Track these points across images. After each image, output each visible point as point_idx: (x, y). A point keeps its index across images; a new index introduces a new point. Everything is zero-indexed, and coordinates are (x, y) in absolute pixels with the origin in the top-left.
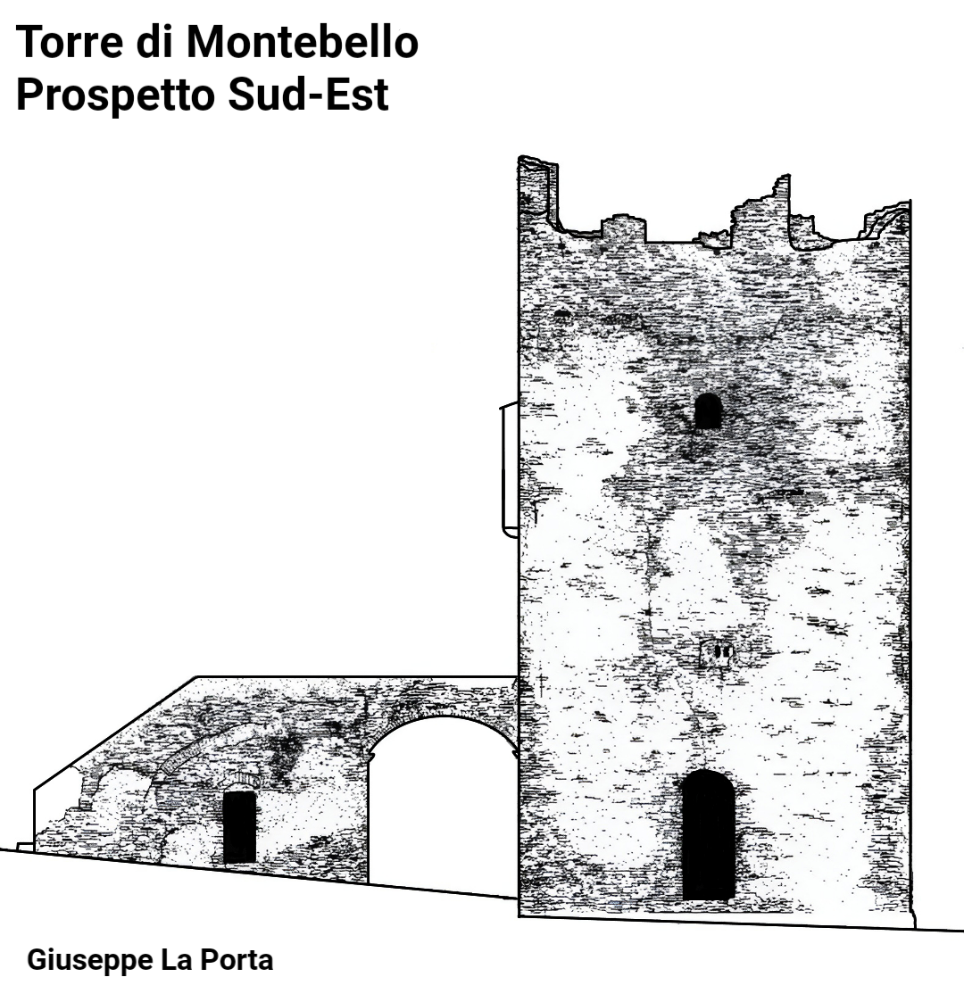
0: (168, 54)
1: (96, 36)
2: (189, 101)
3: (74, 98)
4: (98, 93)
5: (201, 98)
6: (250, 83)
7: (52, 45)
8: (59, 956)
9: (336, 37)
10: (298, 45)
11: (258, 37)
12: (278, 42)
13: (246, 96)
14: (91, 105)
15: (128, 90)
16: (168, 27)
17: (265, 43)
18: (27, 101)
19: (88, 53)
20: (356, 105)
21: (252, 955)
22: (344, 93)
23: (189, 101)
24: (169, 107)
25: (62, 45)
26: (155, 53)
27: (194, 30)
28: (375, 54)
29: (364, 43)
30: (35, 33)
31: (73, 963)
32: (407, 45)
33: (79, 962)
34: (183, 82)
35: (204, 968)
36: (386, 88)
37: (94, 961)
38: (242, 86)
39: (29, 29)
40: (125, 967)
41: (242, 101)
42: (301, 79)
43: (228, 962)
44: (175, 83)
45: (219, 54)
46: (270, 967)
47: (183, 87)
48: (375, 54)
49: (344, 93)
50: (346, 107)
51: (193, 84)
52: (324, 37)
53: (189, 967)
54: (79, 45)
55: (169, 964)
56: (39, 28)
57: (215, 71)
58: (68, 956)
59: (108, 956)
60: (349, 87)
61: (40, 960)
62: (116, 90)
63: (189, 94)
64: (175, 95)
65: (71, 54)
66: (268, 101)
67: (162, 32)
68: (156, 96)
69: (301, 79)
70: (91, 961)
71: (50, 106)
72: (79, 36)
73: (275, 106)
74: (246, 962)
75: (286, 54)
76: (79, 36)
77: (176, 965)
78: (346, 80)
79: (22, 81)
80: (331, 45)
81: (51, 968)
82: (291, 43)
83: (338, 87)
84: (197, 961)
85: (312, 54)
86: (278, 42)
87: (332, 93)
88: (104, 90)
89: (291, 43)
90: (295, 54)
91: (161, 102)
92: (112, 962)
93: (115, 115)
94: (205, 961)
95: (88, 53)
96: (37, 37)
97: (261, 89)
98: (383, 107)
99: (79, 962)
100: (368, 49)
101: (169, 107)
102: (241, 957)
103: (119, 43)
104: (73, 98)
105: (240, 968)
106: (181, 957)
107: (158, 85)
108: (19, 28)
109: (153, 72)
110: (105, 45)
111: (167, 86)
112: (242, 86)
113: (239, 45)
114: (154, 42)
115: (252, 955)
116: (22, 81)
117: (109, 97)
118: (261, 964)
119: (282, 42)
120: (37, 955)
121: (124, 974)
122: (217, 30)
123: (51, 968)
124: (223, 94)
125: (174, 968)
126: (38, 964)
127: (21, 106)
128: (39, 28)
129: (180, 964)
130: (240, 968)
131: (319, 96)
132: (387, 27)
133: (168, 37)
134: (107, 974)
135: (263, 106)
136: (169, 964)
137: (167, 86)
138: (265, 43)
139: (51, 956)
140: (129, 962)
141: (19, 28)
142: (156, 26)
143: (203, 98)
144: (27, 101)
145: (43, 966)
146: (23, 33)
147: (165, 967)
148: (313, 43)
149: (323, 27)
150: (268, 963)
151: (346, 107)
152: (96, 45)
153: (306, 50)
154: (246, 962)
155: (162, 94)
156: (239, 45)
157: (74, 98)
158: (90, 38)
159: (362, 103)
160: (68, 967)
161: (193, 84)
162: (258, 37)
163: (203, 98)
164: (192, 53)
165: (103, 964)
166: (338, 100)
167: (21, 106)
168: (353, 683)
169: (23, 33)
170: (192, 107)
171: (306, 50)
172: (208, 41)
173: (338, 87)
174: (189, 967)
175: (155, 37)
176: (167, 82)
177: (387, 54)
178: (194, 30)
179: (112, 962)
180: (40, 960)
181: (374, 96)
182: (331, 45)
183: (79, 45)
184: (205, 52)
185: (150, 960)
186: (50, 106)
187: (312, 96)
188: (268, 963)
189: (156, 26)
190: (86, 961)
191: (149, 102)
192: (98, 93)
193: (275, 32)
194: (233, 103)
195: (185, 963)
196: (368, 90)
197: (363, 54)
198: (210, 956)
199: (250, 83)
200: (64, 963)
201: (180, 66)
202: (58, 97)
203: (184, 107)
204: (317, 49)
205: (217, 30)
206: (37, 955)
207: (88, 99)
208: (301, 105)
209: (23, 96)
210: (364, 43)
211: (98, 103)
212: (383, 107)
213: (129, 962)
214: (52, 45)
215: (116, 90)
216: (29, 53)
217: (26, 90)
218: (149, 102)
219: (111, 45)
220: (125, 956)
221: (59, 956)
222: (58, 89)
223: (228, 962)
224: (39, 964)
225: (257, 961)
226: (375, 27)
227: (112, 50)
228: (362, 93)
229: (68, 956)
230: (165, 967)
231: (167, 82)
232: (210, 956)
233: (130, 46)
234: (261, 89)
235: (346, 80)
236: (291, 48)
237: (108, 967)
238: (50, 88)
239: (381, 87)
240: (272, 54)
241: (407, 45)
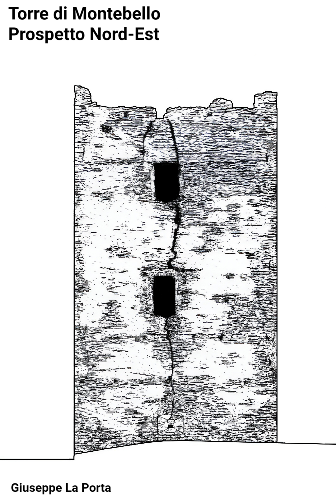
0: (65, 18)
2: (75, 37)
3: (30, 35)
4: (40, 33)
5: (78, 35)
7: (22, 15)
11: (99, 12)
12: (107, 13)
13: (96, 34)
14: (37, 38)
16: (65, 8)
17: (102, 14)
19: (36, 18)
20: (146, 38)
21: (103, 486)
22: (142, 33)
23: (75, 37)
25: (26, 15)
26: (61, 18)
27: (75, 9)
28: (144, 18)
30: (16, 10)
31: (29, 489)
32: (156, 15)
33: (32, 489)
35: (83, 491)
36: (158, 31)
37: (38, 488)
39: (14, 9)
40: (50, 491)
42: (125, 28)
44: (69, 30)
45: (85, 18)
46: (110, 491)
47: (72, 31)
48: (144, 18)
49: (142, 33)
50: (143, 39)
51: (76, 30)
52: (125, 11)
53: (77, 491)
54: (32, 15)
56: (17, 8)
57: (84, 25)
59: (44, 486)
60: (144, 31)
62: (47, 32)
63: (75, 34)
64: (69, 35)
67: (63, 10)
68: (62, 35)
69: (125, 28)
70: (37, 489)
71: (22, 38)
74: (100, 488)
75: (110, 18)
76: (32, 11)
77: (71, 490)
78: (143, 28)
79: (11, 29)
80: (127, 15)
81: (21, 491)
82: (112, 14)
83: (140, 31)
85: (120, 18)
86: (107, 13)
87: (137, 33)
88: (42, 32)
89: (112, 14)
90: (113, 18)
91: (64, 37)
94: (83, 488)
95: (36, 18)
96: (17, 11)
98: (157, 39)
99: (32, 489)
100: (141, 17)
103: (47, 14)
104: (30, 35)
105: (97, 491)
107: (63, 30)
108: (10, 8)
110: (41, 15)
111: (66, 31)
113: (92, 15)
114: (60, 14)
115: (103, 486)
116: (11, 29)
117: (44, 35)
119: (109, 14)
120: (15, 486)
121: (50, 493)
122: (84, 9)
123: (21, 491)
124: (88, 34)
126: (15, 489)
127: (11, 39)
128: (17, 8)
130: (97, 491)
131: (132, 35)
133: (65, 12)
134: (43, 493)
137: (66, 31)
138: (102, 14)
139: (21, 486)
141: (10, 8)
142: (61, 8)
143: (80, 35)
146: (11, 10)
147: (67, 491)
149: (124, 8)
150: (109, 489)
151: (143, 39)
154: (100, 488)
155: (64, 34)
156: (92, 15)
157: (30, 35)
158: (36, 12)
159: (149, 37)
160: (27, 491)
161: (76, 30)
162: (99, 12)
163: (80, 35)
164: (74, 18)
165: (42, 490)
166: (140, 36)
167: (11, 39)
169: (11, 10)
170: (76, 39)
171: (118, 17)
172: (81, 13)
173: (140, 31)
174: (77, 491)
175: (60, 12)
176: (66, 29)
177: (148, 18)
178: (75, 9)
181: (153, 35)
182: (127, 15)
183: (32, 15)
184: (80, 18)
186: (22, 38)
187: (130, 35)
188: (109, 489)
189: (61, 8)
190: (35, 488)
192: (40, 33)
193: (106, 10)
195: (75, 489)
196: (151, 32)
197: (139, 18)
200: (26, 489)
201: (70, 23)
202: (24, 35)
203: (73, 39)
204: (122, 17)
205: (84, 9)
206: (15, 486)
207: (36, 36)
208: (125, 38)
210: (140, 14)
211: (40, 37)
212: (157, 39)
214: (22, 15)
215: (47, 32)
216: (14, 18)
217: (12, 32)
219: (44, 15)
220: (50, 486)
221: (24, 486)
224: (16, 490)
225: (104, 488)
226: (144, 8)
227: (44, 17)
228: (149, 33)
229: (28, 486)
230: (67, 491)
232: (14, 31)
233: (51, 15)
235: (143, 28)
236: (112, 16)
237: (44, 491)
239: (156, 31)
240: (105, 18)
241: (156, 15)
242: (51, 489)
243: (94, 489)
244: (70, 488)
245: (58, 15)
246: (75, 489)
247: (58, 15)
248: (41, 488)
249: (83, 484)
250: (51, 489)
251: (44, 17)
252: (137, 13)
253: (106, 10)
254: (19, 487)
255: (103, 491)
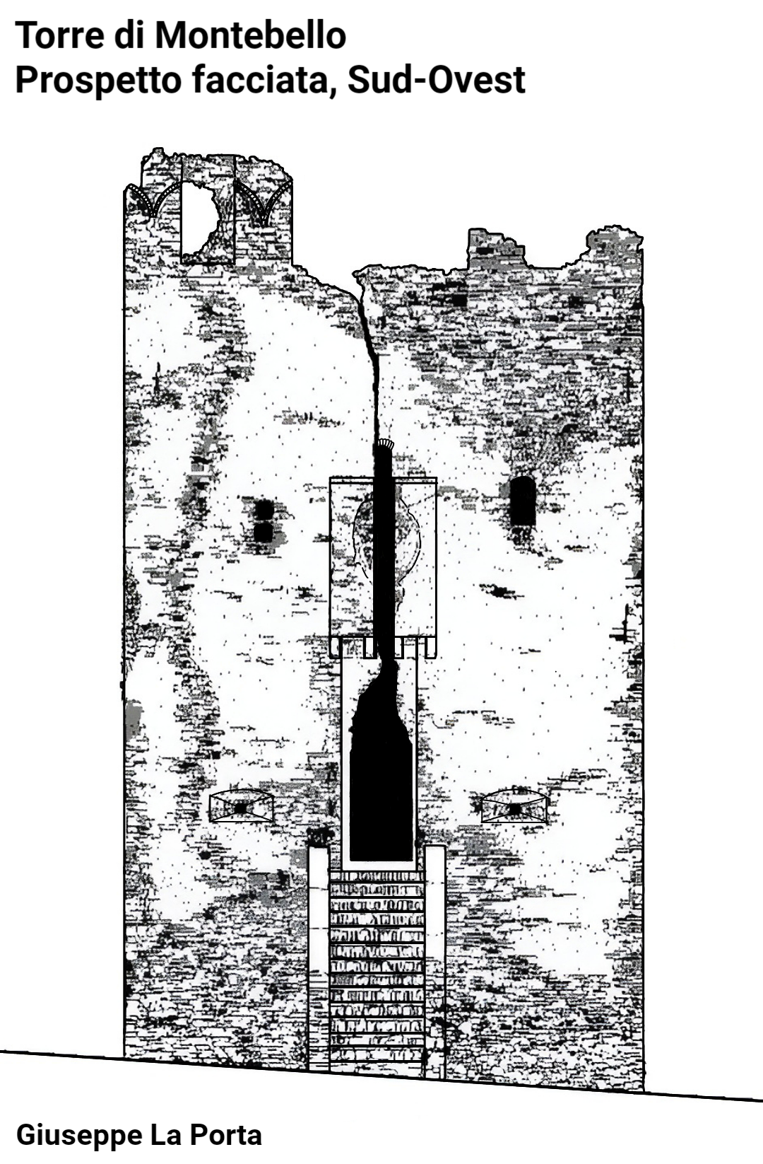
0: (140, 45)
1: (82, 30)
2: (160, 85)
3: (63, 83)
4: (84, 78)
5: (166, 83)
6: (366, 71)
7: (45, 38)
8: (48, 1131)
9: (279, 31)
10: (248, 38)
11: (214, 31)
12: (231, 35)
14: (79, 89)
15: (109, 75)
16: (140, 22)
17: (220, 36)
18: (24, 85)
19: (75, 45)
21: (241, 1130)
23: (160, 85)
24: (143, 90)
25: (54, 38)
27: (161, 26)
28: (311, 45)
29: (302, 37)
30: (31, 28)
31: (61, 1138)
32: (336, 38)
33: (69, 1137)
34: (154, 69)
35: (193, 1143)
37: (83, 1137)
38: (359, 73)
39: (26, 25)
40: (114, 1142)
41: (359, 85)
42: (408, 66)
43: (217, 1137)
44: (148, 70)
45: (182, 45)
46: (259, 1142)
47: (155, 73)
48: (311, 45)
51: (163, 71)
52: (269, 31)
53: (178, 1142)
54: (68, 38)
55: (158, 1140)
56: (35, 23)
57: (180, 60)
58: (57, 1131)
59: (97, 1132)
61: (29, 1135)
62: (99, 76)
63: (160, 79)
64: (148, 81)
65: (61, 45)
66: (381, 85)
67: (136, 26)
68: (132, 81)
69: (408, 66)
70: (80, 1137)
71: (44, 89)
72: (67, 30)
73: (387, 89)
74: (235, 1137)
75: (238, 46)
76: (67, 30)
79: (20, 69)
80: (275, 38)
81: (40, 1143)
82: (242, 35)
84: (186, 1136)
85: (259, 45)
86: (231, 35)
88: (89, 76)
89: (242, 35)
90: (245, 45)
91: (136, 86)
92: (101, 1137)
93: (99, 98)
94: (194, 1136)
95: (75, 45)
96: (33, 31)
97: (375, 75)
98: (520, 90)
99: (69, 1137)
100: (305, 42)
101: (143, 90)
102: (230, 1132)
103: (101, 36)
104: (64, 82)
105: (229, 1143)
106: (170, 1132)
108: (18, 23)
109: (129, 61)
110: (89, 38)
111: (142, 73)
112: (359, 73)
113: (198, 38)
114: (130, 35)
115: (241, 1130)
117: (93, 81)
118: (250, 1140)
119: (235, 36)
120: (26, 1131)
122: (181, 25)
123: (40, 1143)
125: (163, 1143)
127: (20, 89)
128: (35, 23)
129: (169, 1140)
130: (229, 1143)
132: (321, 22)
133: (140, 30)
134: (97, 1149)
135: (377, 90)
136: (158, 1140)
137: (142, 73)
138: (220, 36)
139: (40, 1131)
140: (118, 1137)
141: (18, 23)
142: (131, 22)
143: (172, 83)
144: (24, 85)
145: (32, 1141)
146: (21, 27)
147: (154, 1142)
148: (260, 37)
149: (268, 22)
150: (257, 1138)
152: (82, 37)
153: (254, 42)
154: (235, 1137)
155: (137, 79)
156: (198, 38)
157: (63, 83)
158: (76, 32)
160: (57, 1142)
161: (163, 71)
162: (214, 31)
164: (159, 45)
167: (20, 89)
168: (639, 629)
169: (21, 27)
170: (163, 90)
171: (254, 42)
172: (174, 35)
174: (178, 1142)
176: (142, 69)
177: (320, 45)
178: (161, 26)
179: (101, 1137)
180: (29, 1135)
181: (513, 81)
182: (275, 38)
183: (68, 38)
184: (171, 44)
185: (140, 1136)
186: (44, 89)
187: (418, 81)
188: (257, 1138)
189: (131, 22)
190: (76, 1136)
191: (126, 86)
192: (84, 78)
193: (229, 26)
194: (352, 87)
195: (175, 1138)
196: (508, 76)
197: (301, 45)
198: (199, 1130)
199: (366, 71)
200: (52, 1139)
202: (50, 81)
203: (156, 90)
204: (263, 42)
205: (181, 25)
206: (26, 1131)
207: (76, 84)
208: (408, 89)
209: (21, 81)
210: (302, 37)
212: (520, 90)
213: (118, 1137)
214: (45, 38)
215: (99, 76)
216: (26, 45)
218: (126, 86)
219: (94, 37)
220: (114, 1132)
221: (48, 1131)
222: (50, 75)
223: (217, 1137)
224: (28, 1139)
225: (246, 1136)
226: (311, 22)
227: (95, 42)
229: (57, 1131)
230: (154, 1142)
231: (142, 69)
232: (199, 1130)
234: (375, 75)
236: (242, 40)
237: (97, 1142)
238: (44, 74)
239: (519, 73)
240: (226, 45)
241: (336, 38)
242: (116, 1138)
243: (221, 1137)
244: (162, 1136)
245: (124, 38)
246: (175, 1138)
247: (124, 38)
248: (90, 1136)
249: (194, 1126)
250: (116, 1138)
251: (95, 42)
252: (296, 34)
253: (229, 26)
254: (36, 1133)
255: (242, 1142)
